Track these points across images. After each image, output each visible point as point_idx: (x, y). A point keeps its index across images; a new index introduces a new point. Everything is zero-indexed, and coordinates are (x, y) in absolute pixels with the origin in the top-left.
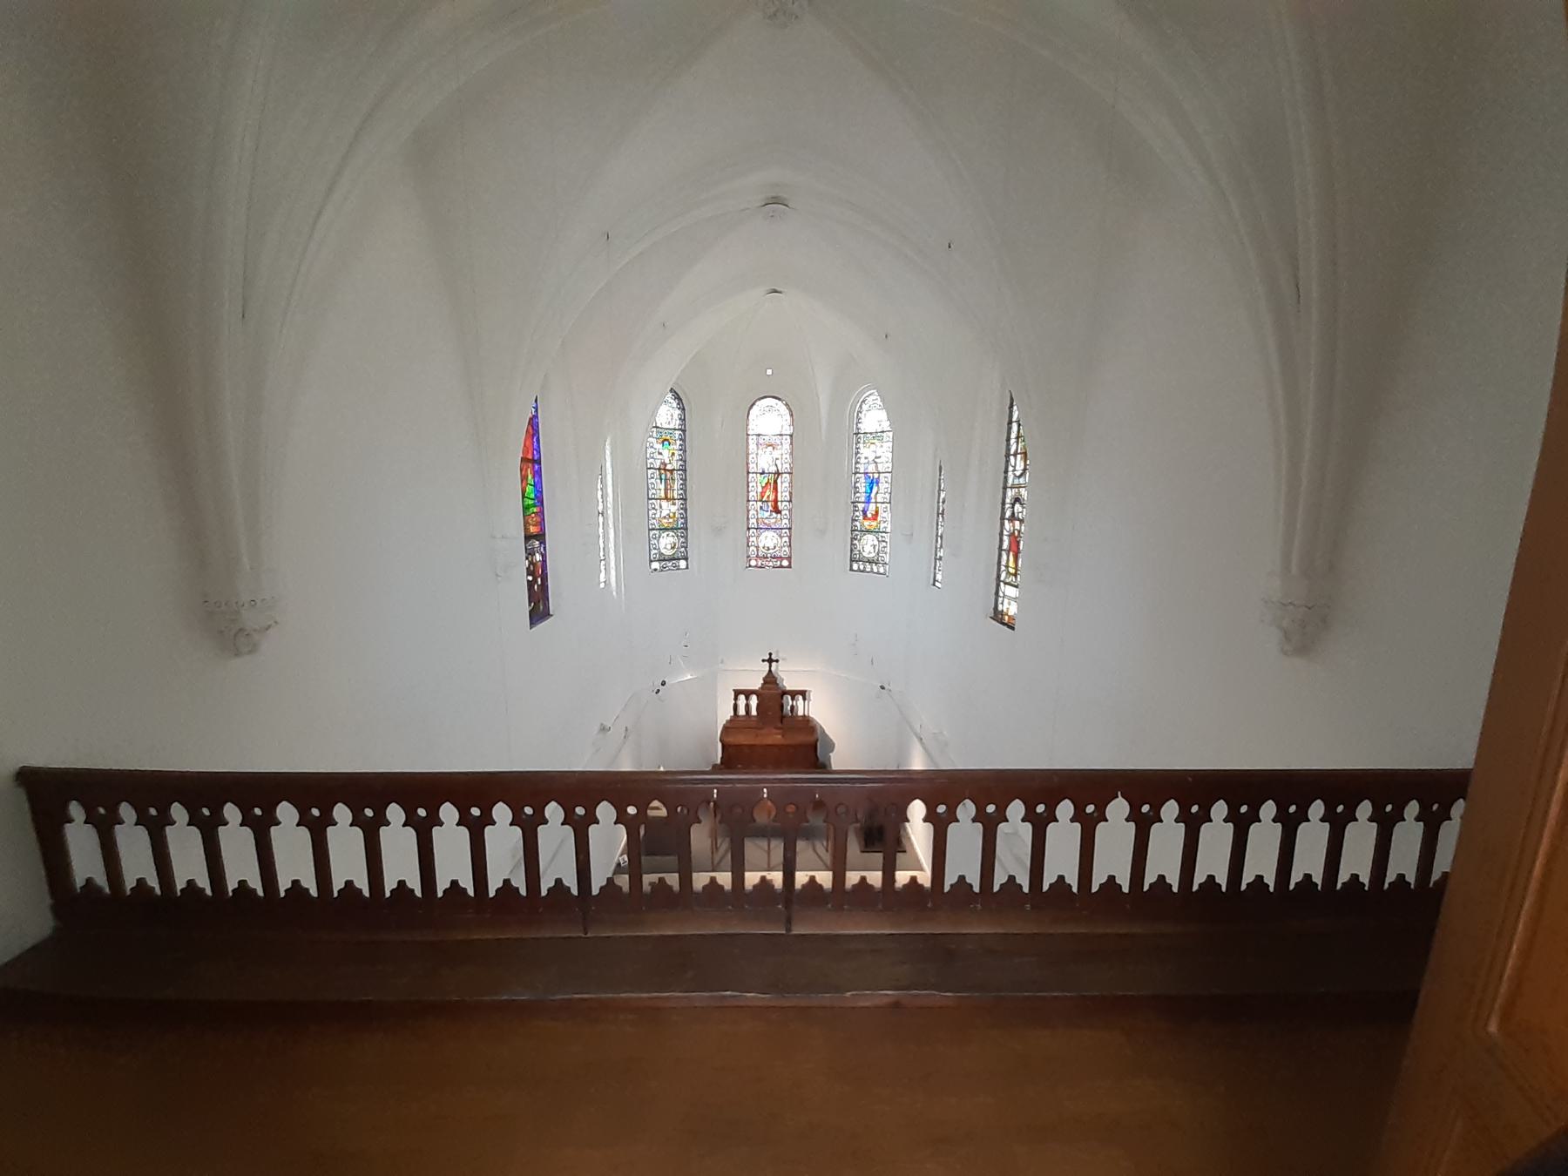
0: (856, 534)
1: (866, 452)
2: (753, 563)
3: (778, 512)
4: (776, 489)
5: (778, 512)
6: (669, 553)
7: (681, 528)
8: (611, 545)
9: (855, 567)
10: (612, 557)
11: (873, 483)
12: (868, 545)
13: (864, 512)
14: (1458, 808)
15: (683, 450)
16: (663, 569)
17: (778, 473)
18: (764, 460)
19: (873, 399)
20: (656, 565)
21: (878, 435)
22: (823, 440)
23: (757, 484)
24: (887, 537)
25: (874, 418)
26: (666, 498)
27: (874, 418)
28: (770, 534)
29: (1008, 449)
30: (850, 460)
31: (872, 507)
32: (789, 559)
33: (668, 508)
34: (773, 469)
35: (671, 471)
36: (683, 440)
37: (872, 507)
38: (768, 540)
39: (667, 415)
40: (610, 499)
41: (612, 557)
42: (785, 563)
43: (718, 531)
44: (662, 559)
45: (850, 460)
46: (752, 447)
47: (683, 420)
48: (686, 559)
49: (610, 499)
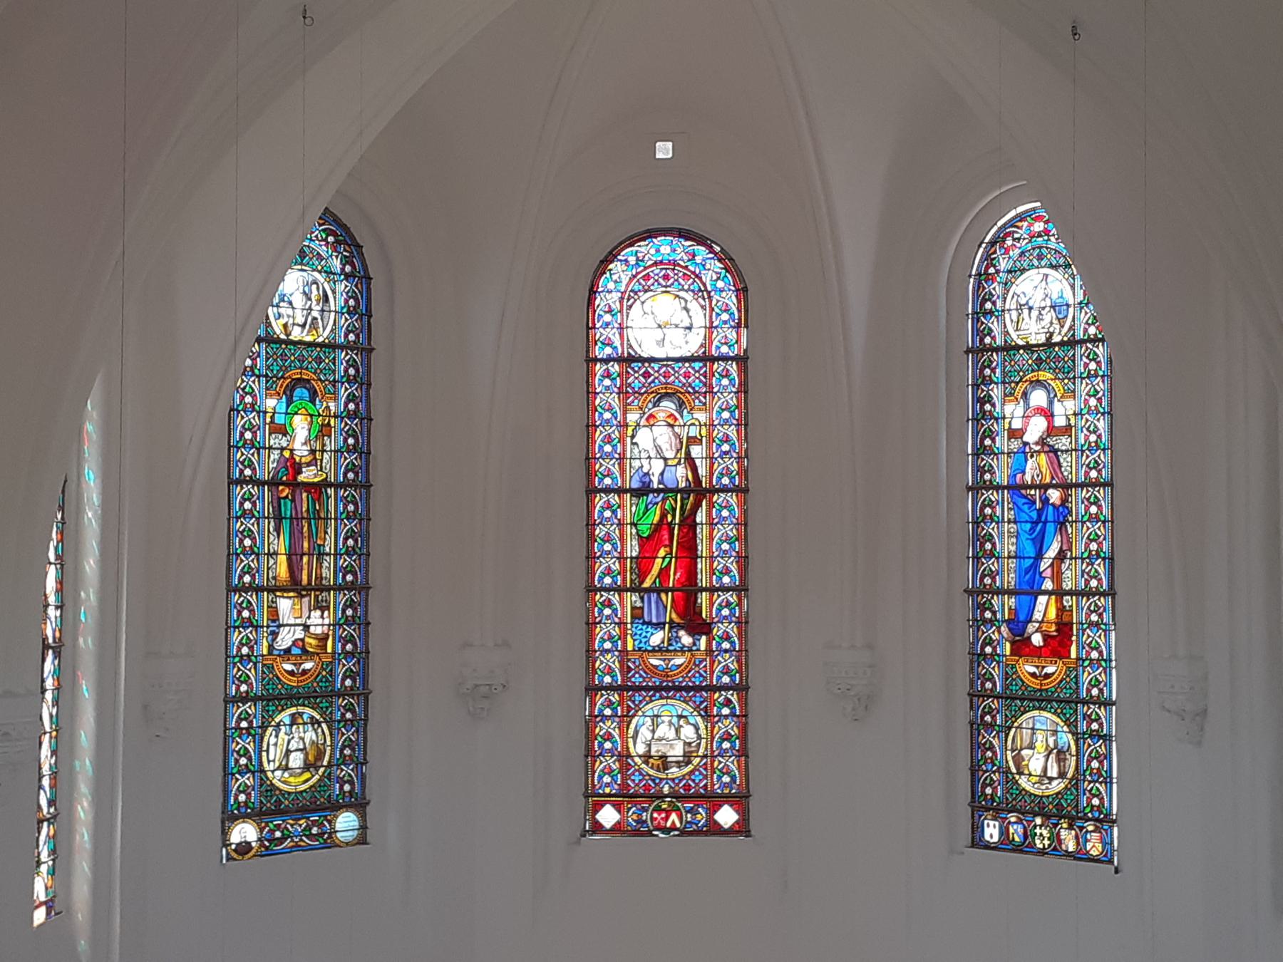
0: (993, 706)
1: (1023, 416)
2: (608, 816)
3: (699, 627)
4: (689, 549)
5: (699, 627)
6: (293, 782)
7: (339, 690)
8: (85, 765)
9: (992, 832)
10: (83, 810)
11: (1046, 519)
12: (1038, 751)
13: (1018, 626)
14: (1116, 829)
15: (361, 415)
16: (268, 846)
17: (698, 491)
18: (653, 447)
19: (1027, 216)
20: (245, 832)
21: (1053, 356)
22: (856, 367)
23: (622, 529)
24: (1110, 720)
25: (1039, 299)
26: (295, 587)
27: (1039, 299)
28: (669, 708)
29: (747, 656)
30: (955, 440)
31: (1045, 608)
32: (740, 801)
33: (297, 620)
34: (681, 474)
35: (316, 489)
36: (362, 380)
37: (1045, 608)
38: (665, 731)
39: (302, 300)
40: (90, 595)
41: (83, 810)
42: (726, 816)
43: (480, 699)
44: (272, 806)
45: (955, 440)
46: (606, 396)
47: (361, 310)
48: (359, 805)
49: (90, 595)
